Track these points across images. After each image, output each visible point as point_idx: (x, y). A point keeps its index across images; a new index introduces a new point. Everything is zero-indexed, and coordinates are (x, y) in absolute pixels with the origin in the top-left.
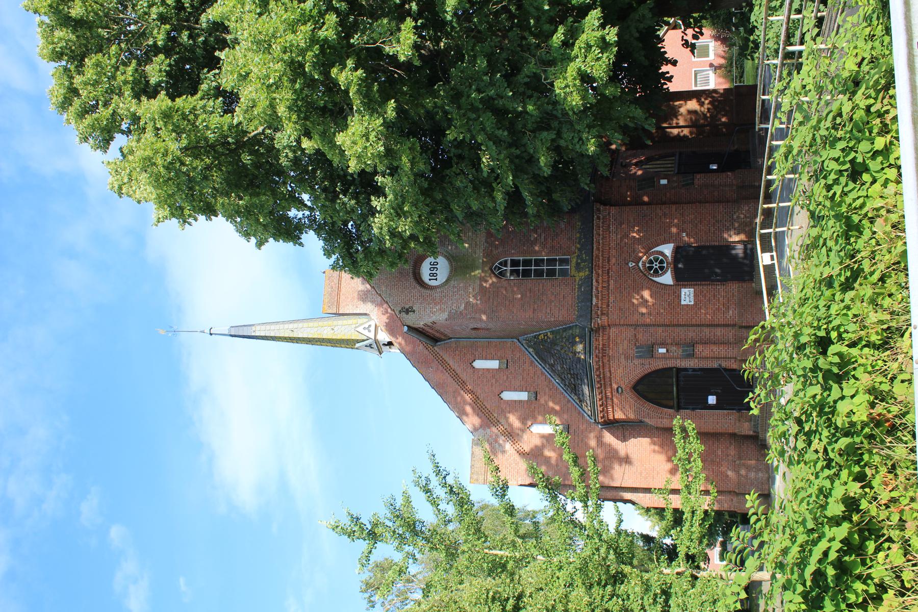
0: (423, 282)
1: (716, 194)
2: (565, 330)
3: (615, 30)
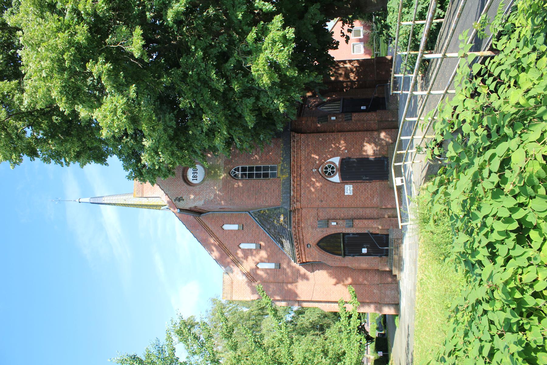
0: (189, 181)
1: (365, 125)
2: (275, 209)
3: (292, 30)
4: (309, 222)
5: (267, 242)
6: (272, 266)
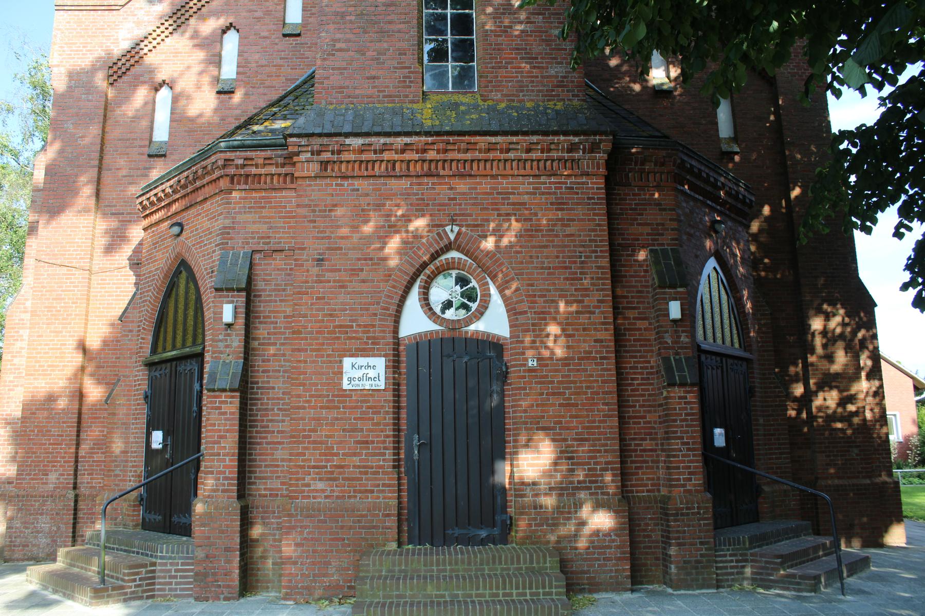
1: (647, 444)
4: (249, 217)
6: (161, 133)
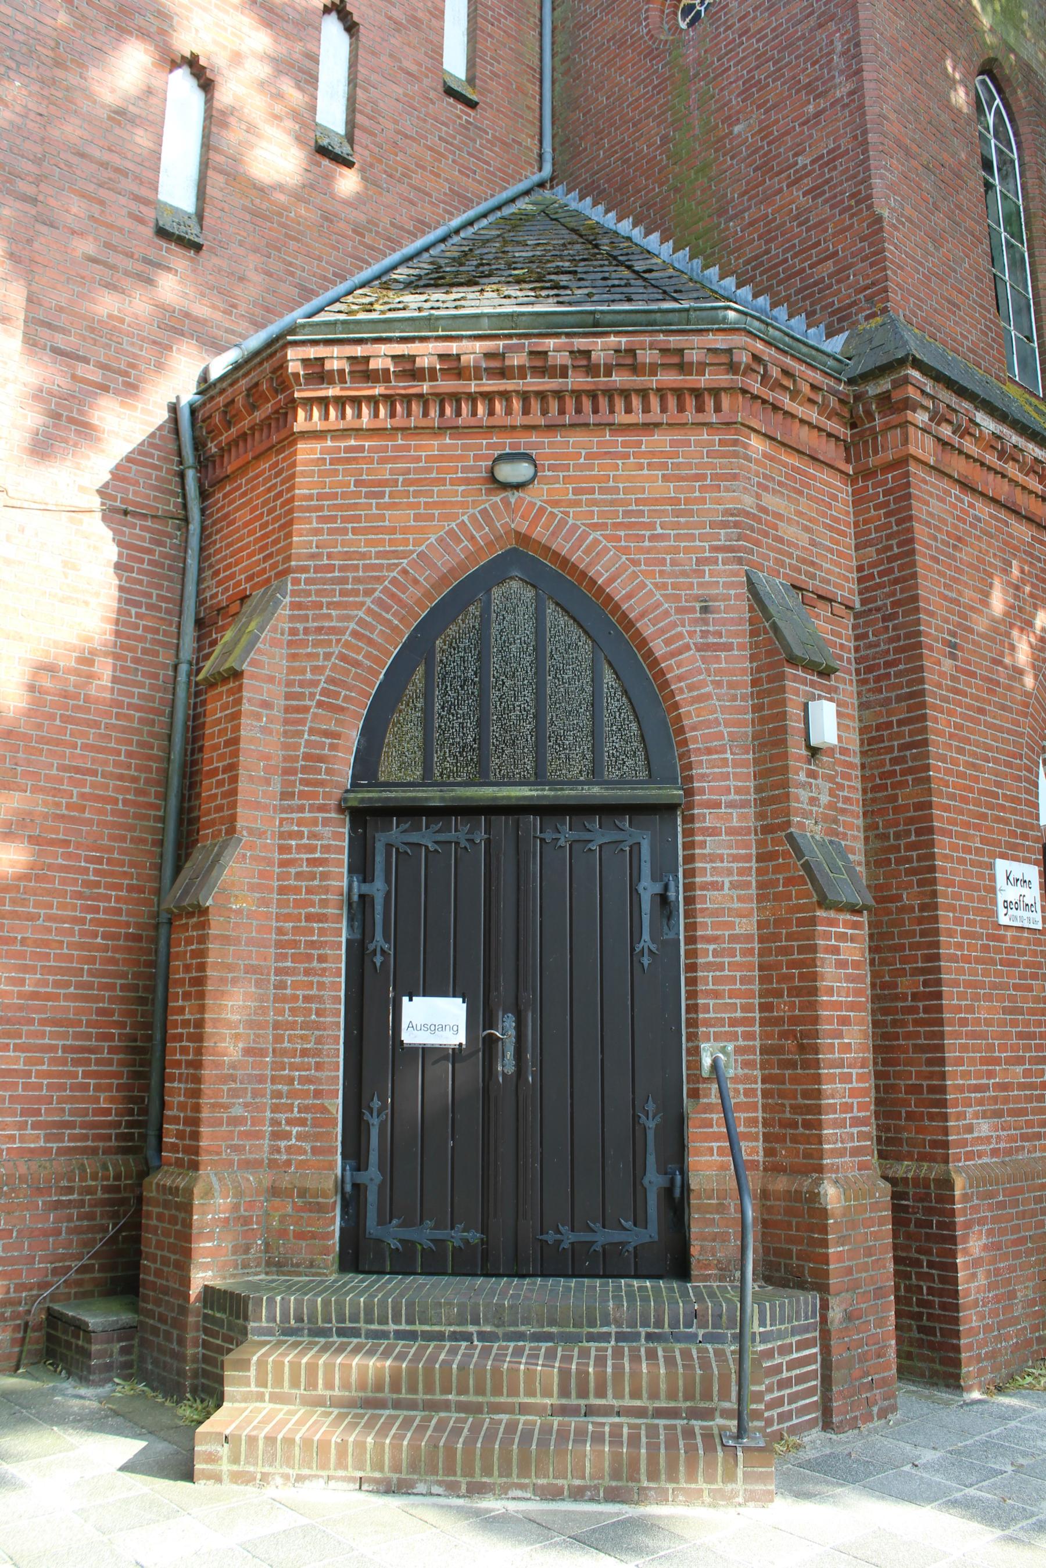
5: (359, 216)
